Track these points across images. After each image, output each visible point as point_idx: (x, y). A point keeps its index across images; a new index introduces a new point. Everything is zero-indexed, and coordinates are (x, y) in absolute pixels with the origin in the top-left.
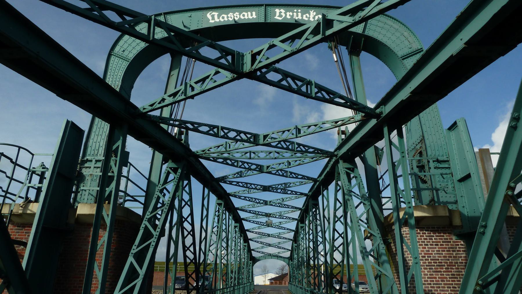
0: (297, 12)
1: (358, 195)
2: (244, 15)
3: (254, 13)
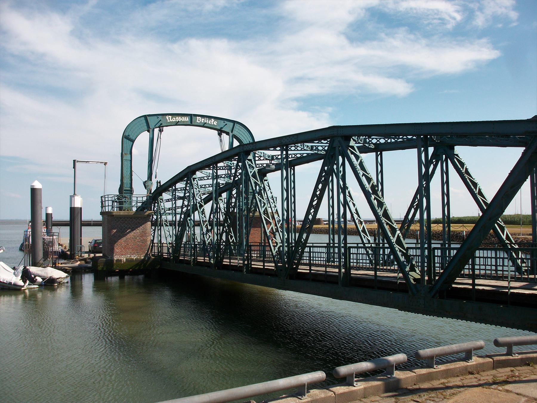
0: (206, 119)
1: (369, 180)
2: (183, 119)
3: (187, 118)
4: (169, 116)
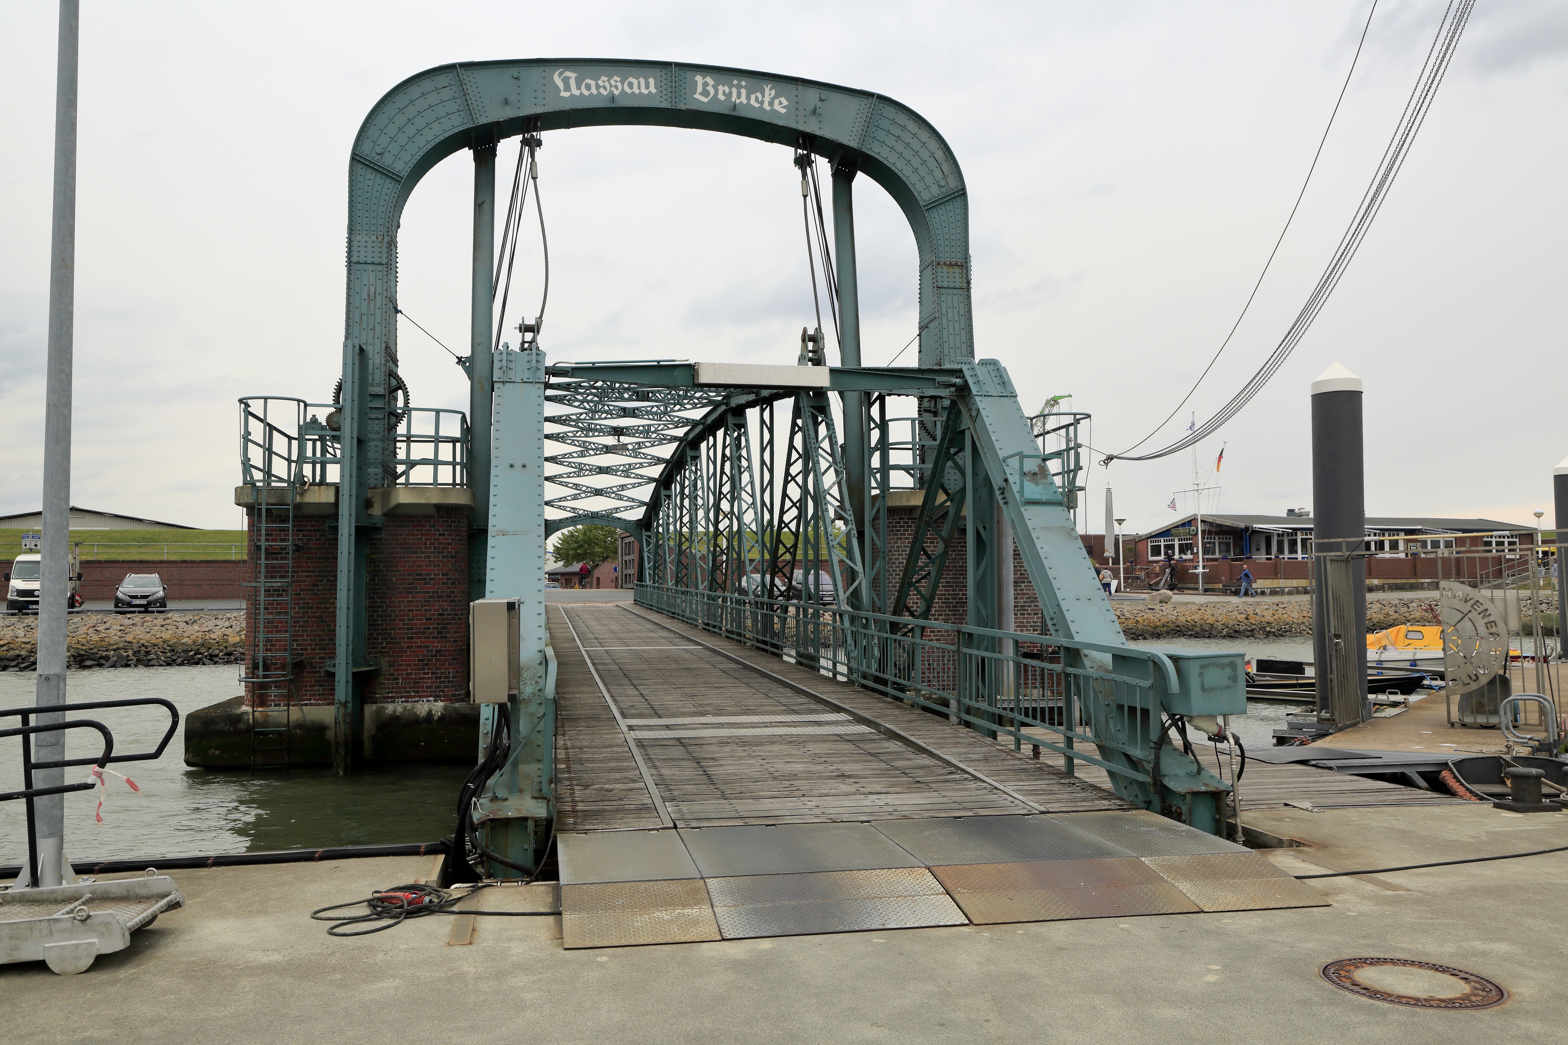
2: (631, 85)
3: (652, 81)
4: (567, 74)
